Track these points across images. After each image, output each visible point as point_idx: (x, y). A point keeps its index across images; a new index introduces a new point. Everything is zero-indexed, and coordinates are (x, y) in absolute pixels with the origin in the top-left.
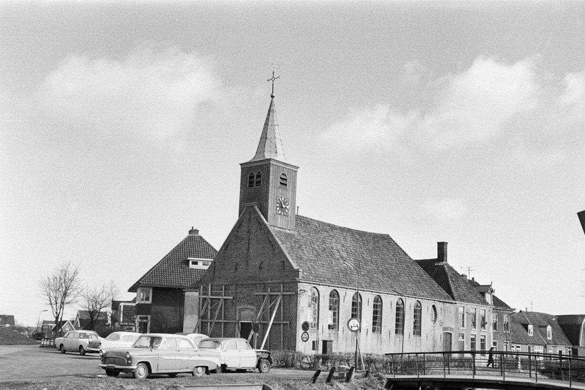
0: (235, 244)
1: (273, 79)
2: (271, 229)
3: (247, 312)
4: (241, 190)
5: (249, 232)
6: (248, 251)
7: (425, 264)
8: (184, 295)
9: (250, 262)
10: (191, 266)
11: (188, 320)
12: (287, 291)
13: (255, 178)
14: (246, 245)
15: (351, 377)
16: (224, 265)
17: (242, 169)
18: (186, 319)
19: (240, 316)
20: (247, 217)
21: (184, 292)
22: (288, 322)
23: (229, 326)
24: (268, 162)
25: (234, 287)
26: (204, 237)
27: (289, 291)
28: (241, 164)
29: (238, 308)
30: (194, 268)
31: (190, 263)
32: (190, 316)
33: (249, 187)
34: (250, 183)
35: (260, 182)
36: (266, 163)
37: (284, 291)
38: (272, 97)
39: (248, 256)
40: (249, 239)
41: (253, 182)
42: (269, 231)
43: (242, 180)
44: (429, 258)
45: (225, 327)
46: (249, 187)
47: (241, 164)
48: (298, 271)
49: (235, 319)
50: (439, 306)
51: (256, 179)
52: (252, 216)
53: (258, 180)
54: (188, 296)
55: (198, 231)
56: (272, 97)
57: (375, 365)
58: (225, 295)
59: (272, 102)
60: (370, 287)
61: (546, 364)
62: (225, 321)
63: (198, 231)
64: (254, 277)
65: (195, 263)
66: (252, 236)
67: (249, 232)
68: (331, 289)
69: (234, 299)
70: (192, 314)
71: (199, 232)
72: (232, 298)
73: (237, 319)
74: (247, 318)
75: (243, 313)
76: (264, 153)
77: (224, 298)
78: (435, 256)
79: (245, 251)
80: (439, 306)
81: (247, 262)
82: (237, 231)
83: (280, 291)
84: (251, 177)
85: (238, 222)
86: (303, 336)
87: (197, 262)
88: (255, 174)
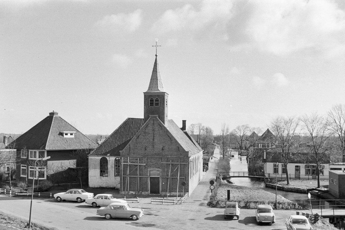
1: (156, 46)
3: (154, 172)
4: (144, 107)
5: (153, 130)
6: (154, 140)
8: (88, 158)
9: (155, 146)
10: (65, 136)
11: (92, 172)
12: (182, 162)
13: (154, 101)
16: (136, 147)
17: (145, 96)
18: (91, 172)
19: (150, 174)
20: (152, 122)
21: (88, 156)
22: (184, 177)
24: (164, 94)
25: (146, 159)
26: (61, 117)
27: (184, 162)
28: (144, 93)
29: (149, 169)
30: (67, 137)
31: (64, 134)
32: (94, 170)
33: (150, 105)
35: (158, 104)
36: (162, 94)
37: (180, 162)
38: (156, 56)
40: (154, 134)
43: (145, 102)
45: (140, 179)
46: (150, 105)
47: (144, 93)
51: (155, 102)
52: (155, 122)
53: (157, 102)
54: (91, 159)
55: (58, 113)
56: (156, 56)
57: (212, 194)
58: (139, 163)
59: (156, 58)
63: (58, 113)
64: (159, 154)
65: (66, 134)
66: (156, 133)
67: (153, 130)
69: (146, 165)
71: (58, 114)
72: (145, 164)
74: (154, 175)
75: (151, 172)
76: (158, 88)
77: (140, 164)
81: (153, 146)
82: (145, 129)
83: (178, 162)
84: (152, 100)
86: (211, 187)
87: (72, 134)
88: (154, 99)
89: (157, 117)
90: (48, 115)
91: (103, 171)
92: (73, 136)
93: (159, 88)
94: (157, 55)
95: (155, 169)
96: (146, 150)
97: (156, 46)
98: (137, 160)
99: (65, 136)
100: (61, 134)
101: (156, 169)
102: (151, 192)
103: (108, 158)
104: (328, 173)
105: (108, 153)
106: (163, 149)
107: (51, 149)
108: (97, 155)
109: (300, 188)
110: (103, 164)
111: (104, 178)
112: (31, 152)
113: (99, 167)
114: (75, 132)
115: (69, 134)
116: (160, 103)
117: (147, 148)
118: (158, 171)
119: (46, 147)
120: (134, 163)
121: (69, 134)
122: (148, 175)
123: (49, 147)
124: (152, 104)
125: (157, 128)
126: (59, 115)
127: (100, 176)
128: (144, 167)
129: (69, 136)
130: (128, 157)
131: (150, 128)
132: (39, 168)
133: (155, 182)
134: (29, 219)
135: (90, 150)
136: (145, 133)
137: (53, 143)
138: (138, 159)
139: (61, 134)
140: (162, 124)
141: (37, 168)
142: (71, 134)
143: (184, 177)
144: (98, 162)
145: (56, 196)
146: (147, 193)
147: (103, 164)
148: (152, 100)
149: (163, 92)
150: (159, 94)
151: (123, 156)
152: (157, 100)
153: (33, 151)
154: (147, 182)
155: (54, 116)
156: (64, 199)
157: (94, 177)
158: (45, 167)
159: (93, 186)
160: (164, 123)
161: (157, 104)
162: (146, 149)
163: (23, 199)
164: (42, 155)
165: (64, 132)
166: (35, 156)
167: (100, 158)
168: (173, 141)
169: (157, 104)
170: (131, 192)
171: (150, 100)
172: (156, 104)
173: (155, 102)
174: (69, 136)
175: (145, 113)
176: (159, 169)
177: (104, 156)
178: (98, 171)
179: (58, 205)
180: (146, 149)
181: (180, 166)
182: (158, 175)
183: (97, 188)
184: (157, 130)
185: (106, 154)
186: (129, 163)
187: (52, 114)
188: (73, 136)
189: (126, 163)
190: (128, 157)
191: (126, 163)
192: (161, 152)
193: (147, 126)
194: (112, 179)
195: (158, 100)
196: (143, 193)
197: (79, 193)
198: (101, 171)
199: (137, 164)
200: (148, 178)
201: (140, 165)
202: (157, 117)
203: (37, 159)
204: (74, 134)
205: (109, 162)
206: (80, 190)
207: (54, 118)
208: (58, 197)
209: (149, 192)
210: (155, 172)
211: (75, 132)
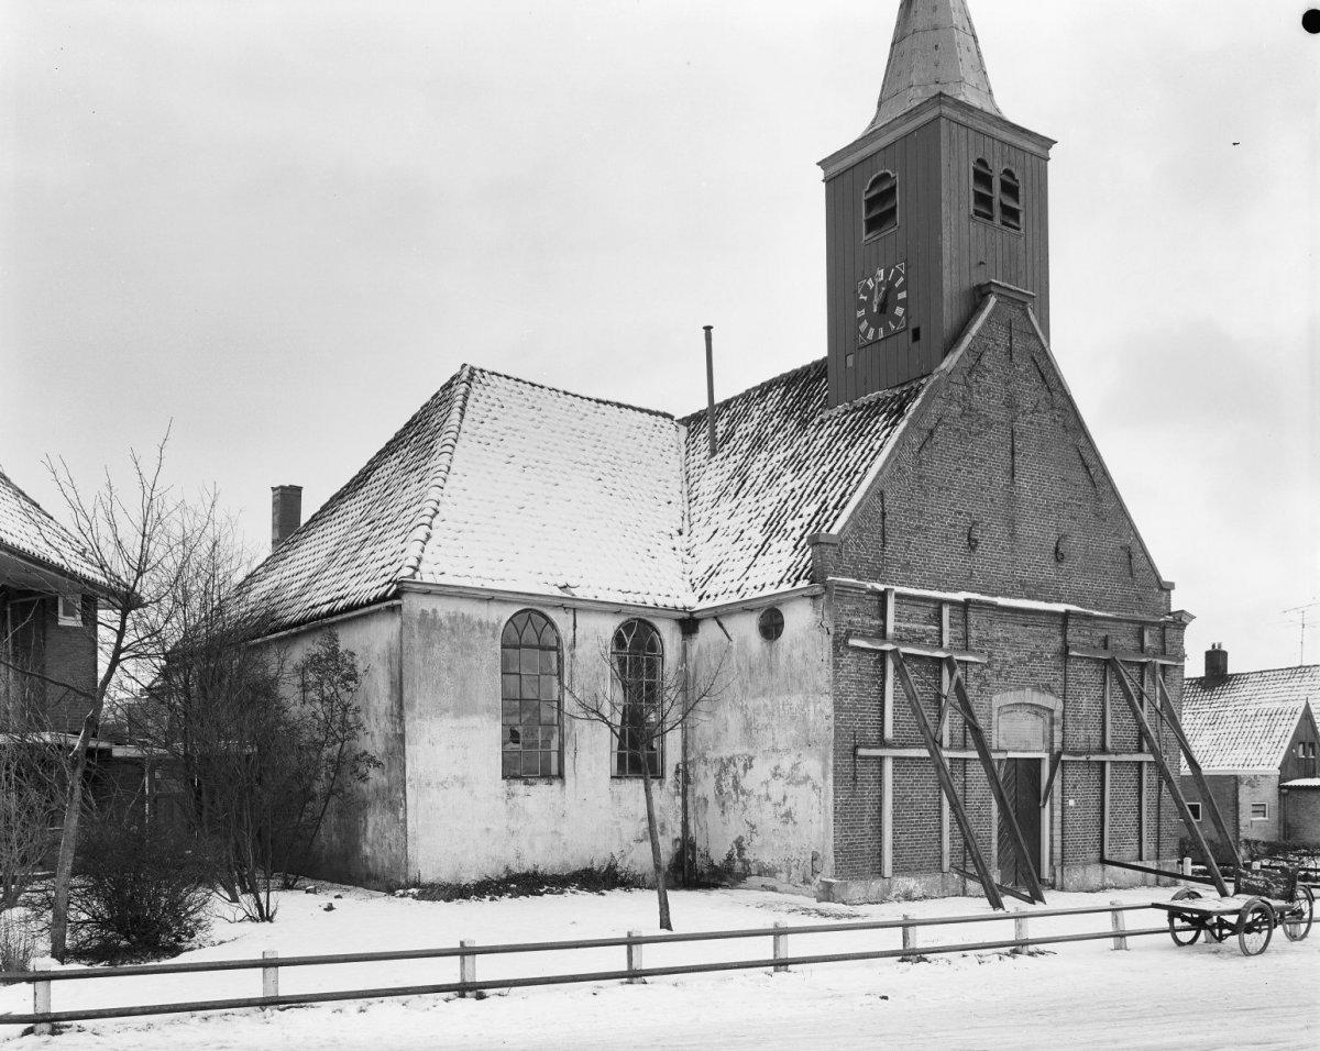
32: (448, 722)
39: (1012, 499)
70: (463, 708)
96: (973, 549)
117: (977, 534)
128: (977, 676)
133: (1022, 788)
178: (485, 739)
180: (972, 544)
205: (573, 656)
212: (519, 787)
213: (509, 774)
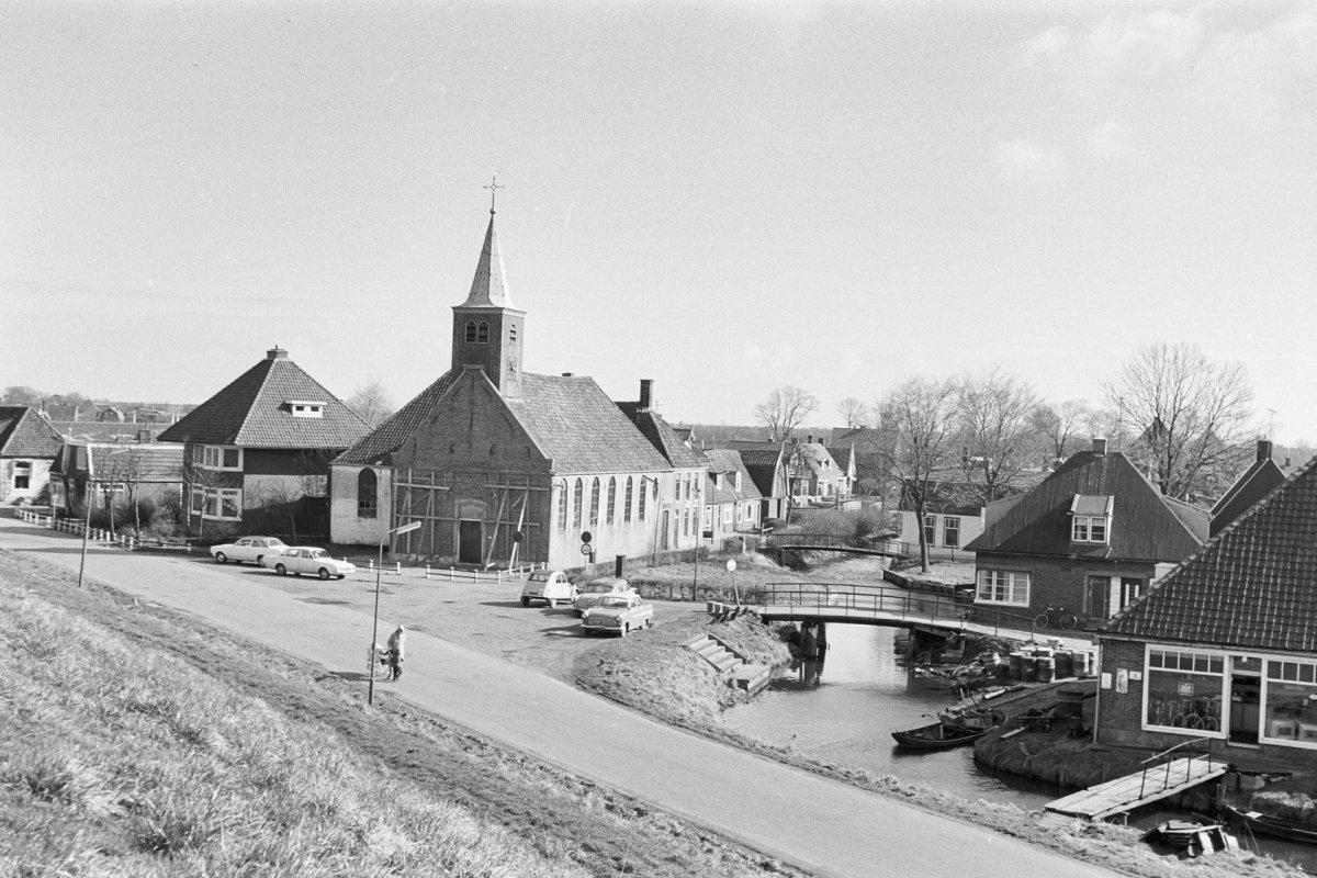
0: (448, 417)
1: (494, 187)
2: (507, 401)
5: (471, 403)
7: (626, 407)
10: (296, 413)
14: (468, 421)
15: (11, 433)
19: (460, 512)
22: (538, 524)
23: (444, 524)
29: (456, 501)
31: (294, 408)
34: (469, 335)
35: (486, 337)
37: (531, 485)
38: (492, 212)
41: (474, 335)
42: (504, 406)
43: (454, 330)
44: (628, 401)
48: (551, 461)
49: (453, 516)
50: (660, 477)
51: (478, 334)
52: (476, 383)
53: (483, 333)
54: (339, 472)
55: (286, 353)
56: (492, 212)
58: (435, 485)
60: (604, 469)
61: (768, 544)
62: (437, 518)
63: (286, 353)
65: (300, 408)
68: (577, 477)
73: (456, 514)
78: (637, 399)
79: (466, 429)
80: (660, 477)
83: (525, 485)
84: (471, 328)
85: (440, 385)
88: (478, 326)
89: (482, 371)
90: (265, 357)
91: (367, 506)
92: (319, 415)
93: (492, 297)
94: (495, 210)
95: (470, 500)
97: (494, 187)
98: (429, 476)
99: (296, 413)
100: (287, 407)
101: (475, 501)
102: (463, 559)
103: (376, 471)
104: (19, 405)
105: (377, 458)
106: (491, 452)
107: (250, 444)
108: (352, 463)
109: (942, 581)
110: (367, 485)
111: (367, 522)
112: (209, 451)
113: (355, 492)
114: (325, 403)
115: (308, 409)
116: (492, 334)
118: (480, 505)
119: (238, 438)
120: (424, 483)
121: (308, 409)
122: (456, 514)
123: (243, 439)
124: (471, 337)
125: (480, 399)
126: (291, 357)
127: (359, 515)
129: (307, 413)
130: (410, 470)
131: (464, 396)
132: (224, 493)
133: (470, 529)
134: (79, 572)
135: (339, 452)
136: (452, 409)
137: (258, 428)
138: (433, 474)
139: (287, 407)
140: (491, 388)
141: (220, 491)
142: (315, 409)
143: (538, 524)
144: (354, 483)
145: (214, 549)
146: (451, 559)
147: (367, 485)
148: (471, 328)
149: (498, 308)
150: (489, 312)
151: (397, 466)
152: (483, 328)
153: (213, 447)
154: (451, 535)
155: (277, 360)
156: (1010, 806)
157: (344, 519)
158: (239, 491)
159: (341, 542)
160: (498, 388)
161: (483, 338)
162: (452, 451)
163: (153, 555)
164: (230, 458)
165: (293, 402)
166: (213, 460)
167: (359, 469)
168: (517, 433)
169: (483, 338)
170: (414, 556)
171: (468, 328)
172: (481, 337)
173: (478, 334)
174: (307, 413)
175: (453, 360)
176: (481, 502)
177: (368, 466)
178: (353, 504)
179: (222, 571)
180: (452, 451)
181: (530, 500)
182: (479, 515)
183: (350, 546)
184: (480, 403)
185: (372, 461)
186: (410, 485)
187: (272, 354)
188: (319, 415)
189: (402, 484)
190: (410, 470)
191: (402, 484)
192: (488, 457)
193: (456, 393)
194: (377, 529)
195: (486, 329)
196: (442, 560)
197: (265, 545)
198: (361, 505)
199: (428, 487)
200: (455, 524)
201: (436, 490)
202: (482, 371)
203: (220, 468)
204: (321, 409)
206: (268, 540)
207: (273, 365)
208: (219, 553)
209: (457, 557)
210: (470, 509)
211: (325, 403)
212: (363, 519)
213: (360, 514)
